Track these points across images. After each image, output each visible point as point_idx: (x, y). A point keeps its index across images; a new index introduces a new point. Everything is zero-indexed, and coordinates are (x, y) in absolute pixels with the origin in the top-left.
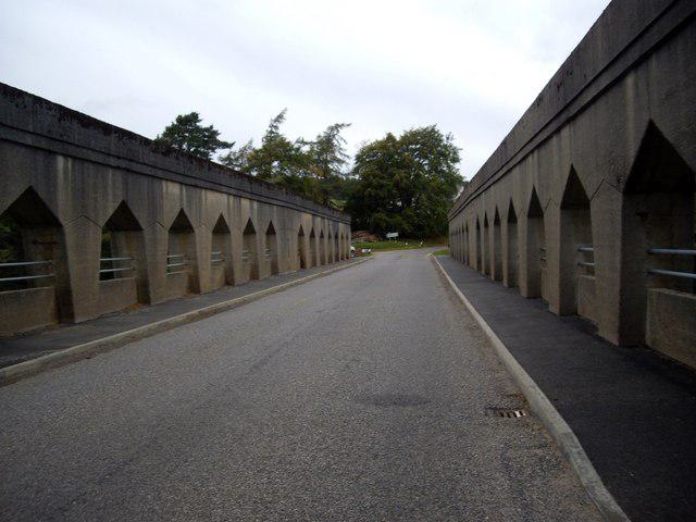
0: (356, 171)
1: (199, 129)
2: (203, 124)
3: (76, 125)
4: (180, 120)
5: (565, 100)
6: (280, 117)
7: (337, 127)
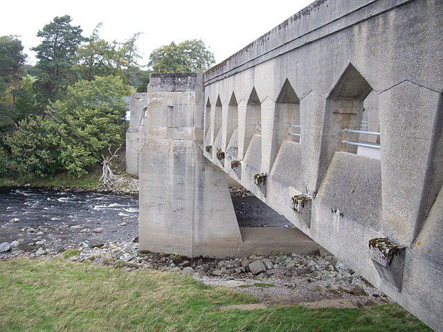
0: (150, 64)
1: (70, 27)
2: (73, 24)
4: (57, 20)
5: (257, 54)
6: (100, 24)
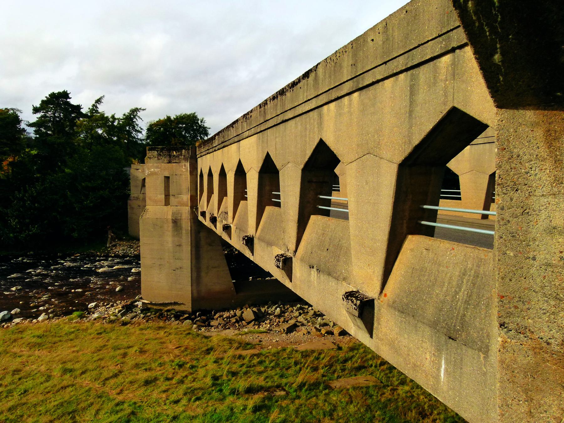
0: (148, 137)
1: (68, 104)
3: (195, 152)
4: (53, 95)
6: (99, 101)
7: (136, 110)
